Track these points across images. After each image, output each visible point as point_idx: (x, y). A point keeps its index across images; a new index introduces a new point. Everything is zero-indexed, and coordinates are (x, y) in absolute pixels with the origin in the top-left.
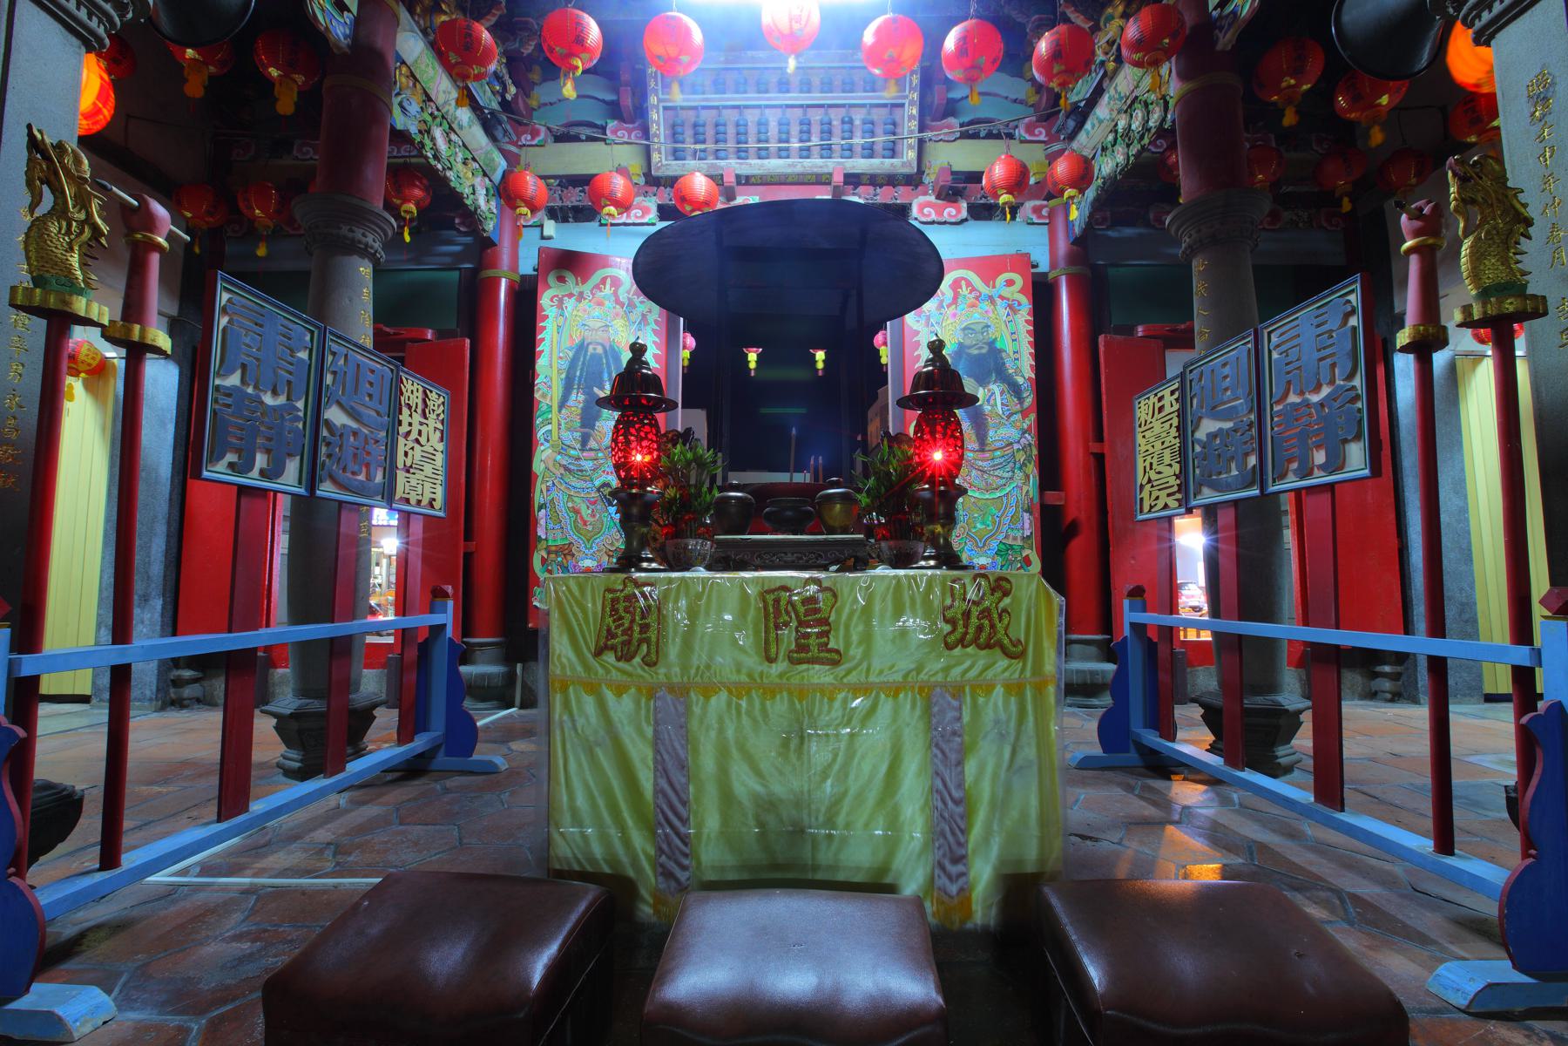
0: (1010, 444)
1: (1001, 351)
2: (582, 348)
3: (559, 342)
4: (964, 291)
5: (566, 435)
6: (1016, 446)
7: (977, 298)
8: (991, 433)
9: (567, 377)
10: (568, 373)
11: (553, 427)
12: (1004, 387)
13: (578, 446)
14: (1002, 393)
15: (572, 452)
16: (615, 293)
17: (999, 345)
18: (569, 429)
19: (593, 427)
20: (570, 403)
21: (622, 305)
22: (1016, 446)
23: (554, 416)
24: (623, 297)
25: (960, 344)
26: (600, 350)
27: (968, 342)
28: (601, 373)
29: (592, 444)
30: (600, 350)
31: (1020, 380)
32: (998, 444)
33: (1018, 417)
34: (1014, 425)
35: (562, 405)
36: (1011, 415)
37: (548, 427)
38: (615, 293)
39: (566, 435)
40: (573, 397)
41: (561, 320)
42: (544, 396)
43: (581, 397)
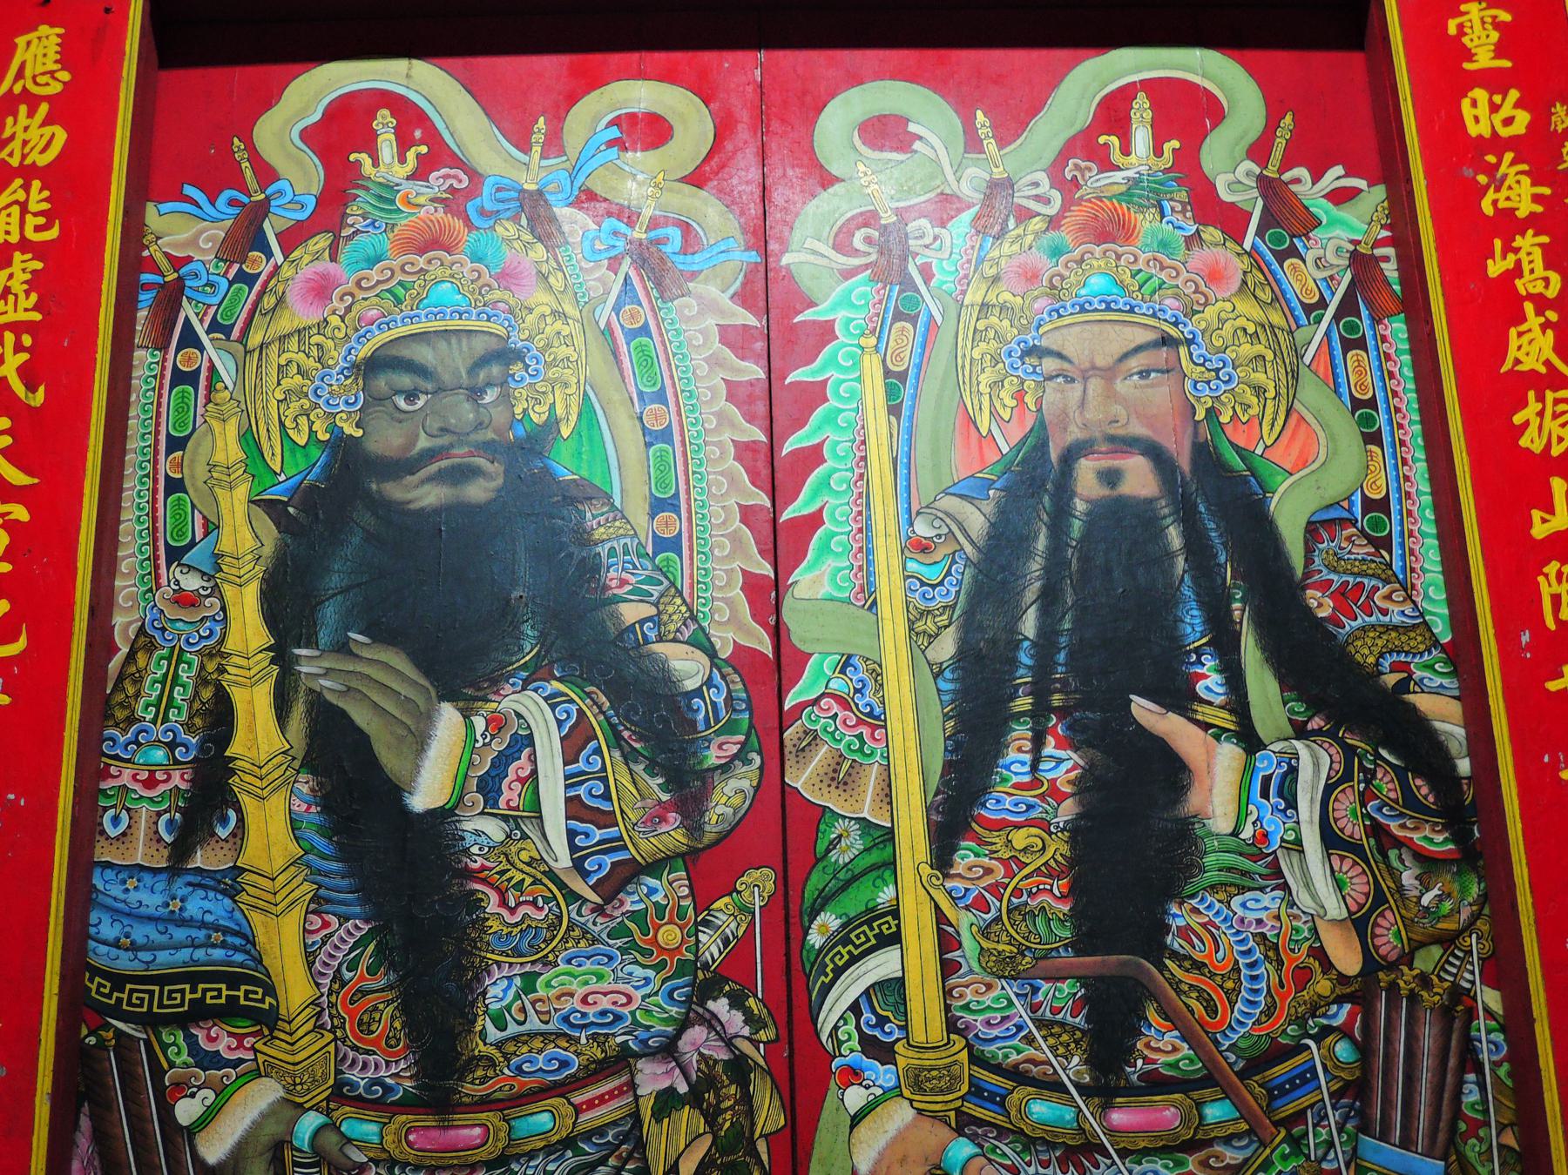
0: (620, 1062)
1: (582, 494)
2: (1037, 477)
3: (902, 465)
4: (386, 162)
5: (992, 1003)
6: (652, 1078)
7: (454, 202)
8: (498, 991)
9: (966, 656)
10: (969, 625)
11: (913, 959)
12: (593, 706)
13: (1074, 1069)
14: (575, 741)
15: (1042, 1110)
16: (1188, 168)
17: (565, 463)
18: (1004, 968)
19: (1151, 939)
20: (1001, 802)
21: (1232, 221)
22: (652, 1078)
23: (912, 892)
24: (1233, 178)
25: (344, 452)
26: (1139, 479)
27: (386, 440)
28: (1162, 606)
29: (1162, 1047)
30: (1139, 479)
31: (688, 667)
32: (541, 1062)
33: (668, 888)
34: (635, 940)
35: (952, 823)
36: (628, 874)
37: (884, 964)
38: (1188, 168)
39: (992, 1003)
40: (1015, 761)
41: (903, 339)
42: (841, 776)
43: (1063, 765)
